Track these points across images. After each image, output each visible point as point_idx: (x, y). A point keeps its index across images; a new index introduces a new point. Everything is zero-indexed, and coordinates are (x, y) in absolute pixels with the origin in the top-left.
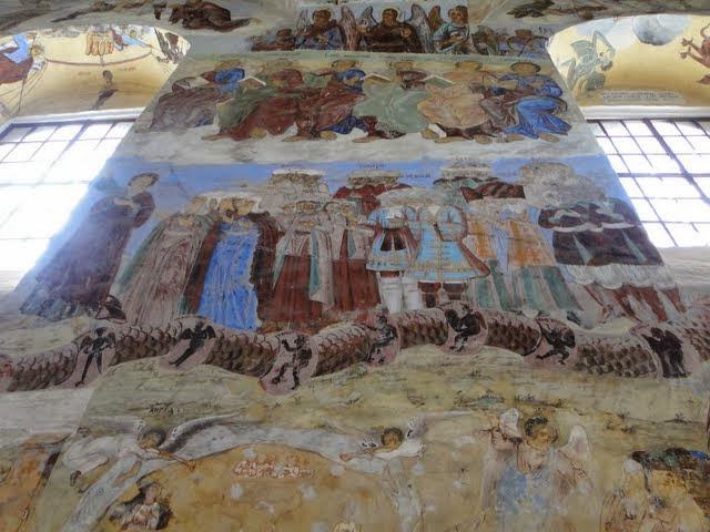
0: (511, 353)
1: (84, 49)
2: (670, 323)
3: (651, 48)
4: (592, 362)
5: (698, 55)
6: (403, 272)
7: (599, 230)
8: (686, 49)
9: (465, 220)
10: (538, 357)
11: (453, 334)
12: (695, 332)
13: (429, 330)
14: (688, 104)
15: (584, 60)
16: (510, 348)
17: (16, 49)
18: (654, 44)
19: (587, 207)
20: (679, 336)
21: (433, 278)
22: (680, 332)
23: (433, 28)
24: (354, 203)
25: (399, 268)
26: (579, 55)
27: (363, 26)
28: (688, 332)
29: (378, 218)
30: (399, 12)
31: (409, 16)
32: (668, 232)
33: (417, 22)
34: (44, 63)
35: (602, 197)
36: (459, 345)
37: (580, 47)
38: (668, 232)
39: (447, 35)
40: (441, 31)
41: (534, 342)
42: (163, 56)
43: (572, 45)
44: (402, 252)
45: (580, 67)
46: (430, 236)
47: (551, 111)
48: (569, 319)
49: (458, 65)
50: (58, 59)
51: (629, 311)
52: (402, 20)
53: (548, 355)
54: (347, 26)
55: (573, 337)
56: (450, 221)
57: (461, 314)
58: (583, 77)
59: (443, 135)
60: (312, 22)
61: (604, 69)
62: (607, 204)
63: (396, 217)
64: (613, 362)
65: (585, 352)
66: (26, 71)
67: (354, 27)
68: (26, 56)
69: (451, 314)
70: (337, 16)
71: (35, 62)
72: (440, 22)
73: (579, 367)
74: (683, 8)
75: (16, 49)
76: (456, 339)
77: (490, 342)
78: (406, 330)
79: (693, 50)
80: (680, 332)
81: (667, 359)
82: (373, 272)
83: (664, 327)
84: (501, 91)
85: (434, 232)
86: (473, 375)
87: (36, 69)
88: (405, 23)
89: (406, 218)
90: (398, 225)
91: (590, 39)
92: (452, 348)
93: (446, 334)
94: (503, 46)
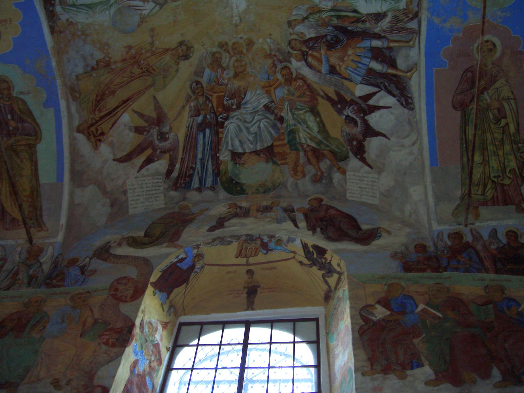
1: (235, 253)
17: (186, 258)
27: (493, 247)
30: (519, 234)
32: (282, 367)
34: (202, 267)
38: (282, 367)
42: (306, 261)
50: (213, 263)
54: (479, 247)
60: (449, 243)
66: (189, 275)
68: (190, 263)
70: (468, 238)
71: (197, 266)
75: (186, 258)
87: (196, 272)
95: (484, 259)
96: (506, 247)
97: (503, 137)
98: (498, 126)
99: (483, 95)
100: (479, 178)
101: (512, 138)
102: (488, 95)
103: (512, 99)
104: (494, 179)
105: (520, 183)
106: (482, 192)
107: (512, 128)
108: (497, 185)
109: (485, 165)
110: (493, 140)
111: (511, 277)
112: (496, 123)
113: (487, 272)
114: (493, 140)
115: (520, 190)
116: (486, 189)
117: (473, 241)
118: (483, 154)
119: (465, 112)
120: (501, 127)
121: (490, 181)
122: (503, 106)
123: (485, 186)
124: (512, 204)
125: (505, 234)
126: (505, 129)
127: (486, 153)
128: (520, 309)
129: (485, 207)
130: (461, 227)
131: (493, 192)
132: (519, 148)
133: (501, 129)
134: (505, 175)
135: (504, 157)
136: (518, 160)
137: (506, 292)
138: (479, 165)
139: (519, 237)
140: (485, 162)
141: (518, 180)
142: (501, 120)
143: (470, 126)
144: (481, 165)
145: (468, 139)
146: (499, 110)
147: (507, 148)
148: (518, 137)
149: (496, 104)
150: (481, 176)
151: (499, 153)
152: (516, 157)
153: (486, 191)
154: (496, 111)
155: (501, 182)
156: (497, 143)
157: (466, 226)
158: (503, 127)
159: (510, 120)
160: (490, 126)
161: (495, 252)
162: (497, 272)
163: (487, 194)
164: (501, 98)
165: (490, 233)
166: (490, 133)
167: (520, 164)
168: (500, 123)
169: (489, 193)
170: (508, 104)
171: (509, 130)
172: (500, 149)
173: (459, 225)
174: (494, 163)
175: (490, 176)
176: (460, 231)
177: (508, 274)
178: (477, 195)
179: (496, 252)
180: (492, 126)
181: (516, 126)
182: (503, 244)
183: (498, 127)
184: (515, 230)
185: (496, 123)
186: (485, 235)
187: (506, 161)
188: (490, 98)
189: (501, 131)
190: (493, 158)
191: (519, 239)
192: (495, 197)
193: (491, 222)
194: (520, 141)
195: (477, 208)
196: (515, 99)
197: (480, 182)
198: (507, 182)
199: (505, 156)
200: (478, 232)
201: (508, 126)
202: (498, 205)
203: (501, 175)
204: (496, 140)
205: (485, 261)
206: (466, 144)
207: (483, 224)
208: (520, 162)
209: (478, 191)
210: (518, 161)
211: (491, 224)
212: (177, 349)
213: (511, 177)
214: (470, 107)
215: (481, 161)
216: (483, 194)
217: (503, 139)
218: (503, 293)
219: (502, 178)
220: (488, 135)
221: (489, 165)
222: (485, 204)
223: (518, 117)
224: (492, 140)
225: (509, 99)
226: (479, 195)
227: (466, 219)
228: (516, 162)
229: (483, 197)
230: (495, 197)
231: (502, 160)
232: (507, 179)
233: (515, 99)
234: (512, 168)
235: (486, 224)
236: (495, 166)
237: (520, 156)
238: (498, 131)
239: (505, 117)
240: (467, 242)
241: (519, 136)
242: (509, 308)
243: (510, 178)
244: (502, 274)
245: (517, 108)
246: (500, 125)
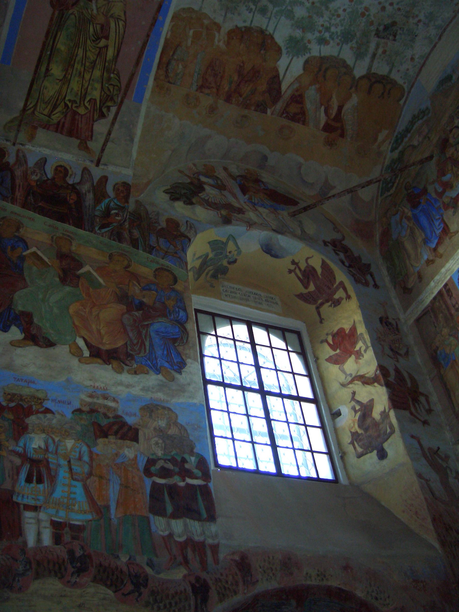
0: (106, 589)
2: (208, 573)
3: (268, 257)
4: (155, 601)
5: (300, 275)
6: (40, 507)
7: (182, 484)
8: (292, 267)
9: (91, 459)
10: (123, 594)
11: (71, 569)
12: (220, 580)
13: (54, 565)
14: (285, 314)
15: (216, 255)
16: (106, 585)
18: (272, 255)
19: (179, 459)
20: (210, 583)
21: (61, 516)
22: (211, 580)
23: (98, 201)
24: (6, 423)
25: (39, 504)
26: (213, 250)
27: (34, 177)
28: (216, 579)
29: (25, 445)
30: (70, 172)
31: (77, 179)
33: (85, 188)
35: (192, 453)
36: (73, 580)
37: (214, 245)
39: (107, 213)
40: (103, 205)
41: (122, 581)
43: (209, 243)
44: (41, 486)
45: (211, 259)
46: (63, 474)
47: (175, 340)
48: (148, 564)
49: (111, 256)
51: (186, 562)
52: (71, 182)
53: (129, 594)
54: (18, 173)
55: (147, 580)
56: (80, 459)
57: (79, 553)
58: (211, 268)
59: (87, 353)
61: (229, 263)
62: (193, 459)
63: (39, 447)
64: (167, 602)
65: (153, 593)
67: (25, 176)
69: (71, 553)
72: (105, 195)
73: (147, 604)
74: (299, 232)
76: (73, 574)
77: (95, 580)
78: (38, 563)
79: (297, 271)
80: (211, 580)
81: (199, 601)
82: (18, 504)
83: (204, 575)
84: (141, 306)
85: (67, 470)
86: (80, 606)
88: (73, 185)
89: (47, 450)
90: (40, 456)
91: (224, 240)
92: (69, 582)
93: (66, 569)
94: (153, 240)
95: (17, 187)
96: (49, 182)
97: (96, 60)
98: (95, 45)
99: (90, 3)
100: (51, 96)
101: (107, 64)
102: (96, 6)
103: (121, 20)
104: (68, 103)
105: (96, 117)
106: (48, 112)
107: (110, 53)
108: (69, 110)
109: (64, 84)
110: (84, 58)
111: (37, 216)
112: (93, 41)
113: (13, 203)
114: (84, 58)
115: (93, 125)
116: (55, 110)
117: (15, 164)
118: (67, 70)
119: (63, 15)
120: (98, 47)
121: (63, 104)
122: (108, 24)
123: (55, 107)
124: (77, 138)
125: (54, 167)
126: (101, 52)
127: (70, 71)
128: (25, 253)
129: (45, 130)
130: (8, 143)
131: (62, 116)
132: (109, 79)
133: (97, 49)
134: (82, 103)
135: (89, 83)
136: (104, 92)
137: (21, 230)
138: (58, 81)
139: (69, 175)
140: (65, 80)
141: (95, 114)
142: (101, 40)
143: (63, 32)
144: (60, 81)
145: (56, 47)
146: (102, 26)
147: (97, 73)
148: (113, 66)
149: (101, 19)
150: (54, 95)
151: (85, 76)
152: (102, 88)
153: (54, 113)
154: (98, 27)
155: (75, 109)
156: (87, 64)
157: (14, 144)
158: (100, 48)
159: (111, 42)
160: (86, 42)
161: (34, 184)
162: (24, 206)
163: (53, 117)
164: (110, 14)
165: (39, 161)
166: (84, 49)
167: (105, 97)
168: (99, 42)
169: (56, 117)
170: (116, 24)
171: (106, 54)
172: (89, 72)
173: (7, 140)
174: (75, 85)
175: (65, 98)
176: (5, 148)
177: (35, 212)
178: (42, 114)
179: (35, 184)
180: (88, 41)
181: (115, 54)
182: (47, 177)
183: (94, 46)
184: (68, 168)
185: (93, 41)
186: (31, 162)
187: (90, 87)
188: (97, 9)
189: (97, 52)
190: (77, 79)
191: (67, 178)
192: (61, 124)
193: (45, 149)
194: (114, 70)
195: (35, 128)
196: (125, 22)
197: (51, 101)
198: (82, 111)
199: (91, 82)
200: (24, 156)
201: (107, 49)
202: (61, 133)
203: (78, 102)
204: (87, 60)
205: (17, 190)
206: (51, 52)
207: (33, 149)
208: (105, 95)
209: (44, 110)
210: (103, 93)
211: (44, 152)
212: (280, 332)
213: (89, 107)
214: (71, 12)
215: (61, 78)
216: (49, 116)
217: (95, 62)
218: (18, 229)
219: (77, 105)
220: (80, 52)
221: (68, 86)
222: (46, 127)
223: (122, 43)
224: (83, 58)
225: (119, 18)
226: (45, 115)
227: (16, 137)
228: (101, 92)
229: (47, 118)
230: (61, 124)
231: (86, 85)
232: (83, 107)
233: (125, 22)
234: (94, 98)
235: (38, 149)
236: (76, 89)
237: (108, 87)
238: (93, 51)
239: (107, 38)
240: (8, 163)
241: (115, 66)
242: (13, 248)
243: (86, 108)
244: (30, 210)
245: (124, 32)
246: (97, 44)
